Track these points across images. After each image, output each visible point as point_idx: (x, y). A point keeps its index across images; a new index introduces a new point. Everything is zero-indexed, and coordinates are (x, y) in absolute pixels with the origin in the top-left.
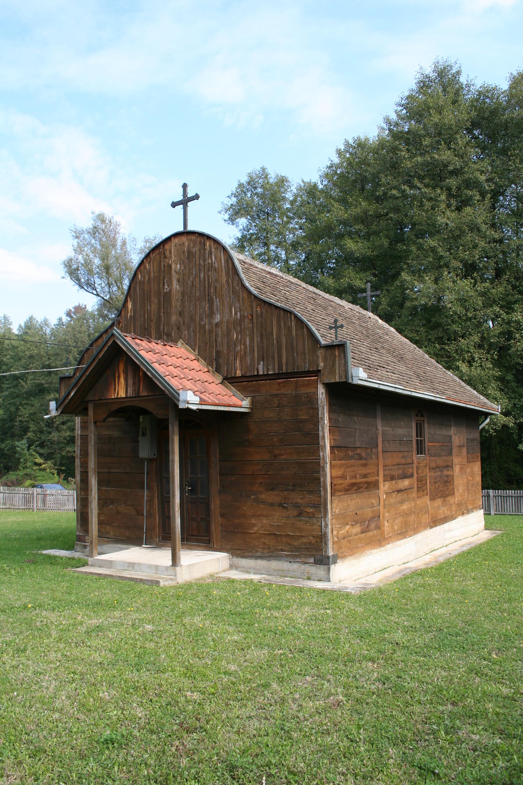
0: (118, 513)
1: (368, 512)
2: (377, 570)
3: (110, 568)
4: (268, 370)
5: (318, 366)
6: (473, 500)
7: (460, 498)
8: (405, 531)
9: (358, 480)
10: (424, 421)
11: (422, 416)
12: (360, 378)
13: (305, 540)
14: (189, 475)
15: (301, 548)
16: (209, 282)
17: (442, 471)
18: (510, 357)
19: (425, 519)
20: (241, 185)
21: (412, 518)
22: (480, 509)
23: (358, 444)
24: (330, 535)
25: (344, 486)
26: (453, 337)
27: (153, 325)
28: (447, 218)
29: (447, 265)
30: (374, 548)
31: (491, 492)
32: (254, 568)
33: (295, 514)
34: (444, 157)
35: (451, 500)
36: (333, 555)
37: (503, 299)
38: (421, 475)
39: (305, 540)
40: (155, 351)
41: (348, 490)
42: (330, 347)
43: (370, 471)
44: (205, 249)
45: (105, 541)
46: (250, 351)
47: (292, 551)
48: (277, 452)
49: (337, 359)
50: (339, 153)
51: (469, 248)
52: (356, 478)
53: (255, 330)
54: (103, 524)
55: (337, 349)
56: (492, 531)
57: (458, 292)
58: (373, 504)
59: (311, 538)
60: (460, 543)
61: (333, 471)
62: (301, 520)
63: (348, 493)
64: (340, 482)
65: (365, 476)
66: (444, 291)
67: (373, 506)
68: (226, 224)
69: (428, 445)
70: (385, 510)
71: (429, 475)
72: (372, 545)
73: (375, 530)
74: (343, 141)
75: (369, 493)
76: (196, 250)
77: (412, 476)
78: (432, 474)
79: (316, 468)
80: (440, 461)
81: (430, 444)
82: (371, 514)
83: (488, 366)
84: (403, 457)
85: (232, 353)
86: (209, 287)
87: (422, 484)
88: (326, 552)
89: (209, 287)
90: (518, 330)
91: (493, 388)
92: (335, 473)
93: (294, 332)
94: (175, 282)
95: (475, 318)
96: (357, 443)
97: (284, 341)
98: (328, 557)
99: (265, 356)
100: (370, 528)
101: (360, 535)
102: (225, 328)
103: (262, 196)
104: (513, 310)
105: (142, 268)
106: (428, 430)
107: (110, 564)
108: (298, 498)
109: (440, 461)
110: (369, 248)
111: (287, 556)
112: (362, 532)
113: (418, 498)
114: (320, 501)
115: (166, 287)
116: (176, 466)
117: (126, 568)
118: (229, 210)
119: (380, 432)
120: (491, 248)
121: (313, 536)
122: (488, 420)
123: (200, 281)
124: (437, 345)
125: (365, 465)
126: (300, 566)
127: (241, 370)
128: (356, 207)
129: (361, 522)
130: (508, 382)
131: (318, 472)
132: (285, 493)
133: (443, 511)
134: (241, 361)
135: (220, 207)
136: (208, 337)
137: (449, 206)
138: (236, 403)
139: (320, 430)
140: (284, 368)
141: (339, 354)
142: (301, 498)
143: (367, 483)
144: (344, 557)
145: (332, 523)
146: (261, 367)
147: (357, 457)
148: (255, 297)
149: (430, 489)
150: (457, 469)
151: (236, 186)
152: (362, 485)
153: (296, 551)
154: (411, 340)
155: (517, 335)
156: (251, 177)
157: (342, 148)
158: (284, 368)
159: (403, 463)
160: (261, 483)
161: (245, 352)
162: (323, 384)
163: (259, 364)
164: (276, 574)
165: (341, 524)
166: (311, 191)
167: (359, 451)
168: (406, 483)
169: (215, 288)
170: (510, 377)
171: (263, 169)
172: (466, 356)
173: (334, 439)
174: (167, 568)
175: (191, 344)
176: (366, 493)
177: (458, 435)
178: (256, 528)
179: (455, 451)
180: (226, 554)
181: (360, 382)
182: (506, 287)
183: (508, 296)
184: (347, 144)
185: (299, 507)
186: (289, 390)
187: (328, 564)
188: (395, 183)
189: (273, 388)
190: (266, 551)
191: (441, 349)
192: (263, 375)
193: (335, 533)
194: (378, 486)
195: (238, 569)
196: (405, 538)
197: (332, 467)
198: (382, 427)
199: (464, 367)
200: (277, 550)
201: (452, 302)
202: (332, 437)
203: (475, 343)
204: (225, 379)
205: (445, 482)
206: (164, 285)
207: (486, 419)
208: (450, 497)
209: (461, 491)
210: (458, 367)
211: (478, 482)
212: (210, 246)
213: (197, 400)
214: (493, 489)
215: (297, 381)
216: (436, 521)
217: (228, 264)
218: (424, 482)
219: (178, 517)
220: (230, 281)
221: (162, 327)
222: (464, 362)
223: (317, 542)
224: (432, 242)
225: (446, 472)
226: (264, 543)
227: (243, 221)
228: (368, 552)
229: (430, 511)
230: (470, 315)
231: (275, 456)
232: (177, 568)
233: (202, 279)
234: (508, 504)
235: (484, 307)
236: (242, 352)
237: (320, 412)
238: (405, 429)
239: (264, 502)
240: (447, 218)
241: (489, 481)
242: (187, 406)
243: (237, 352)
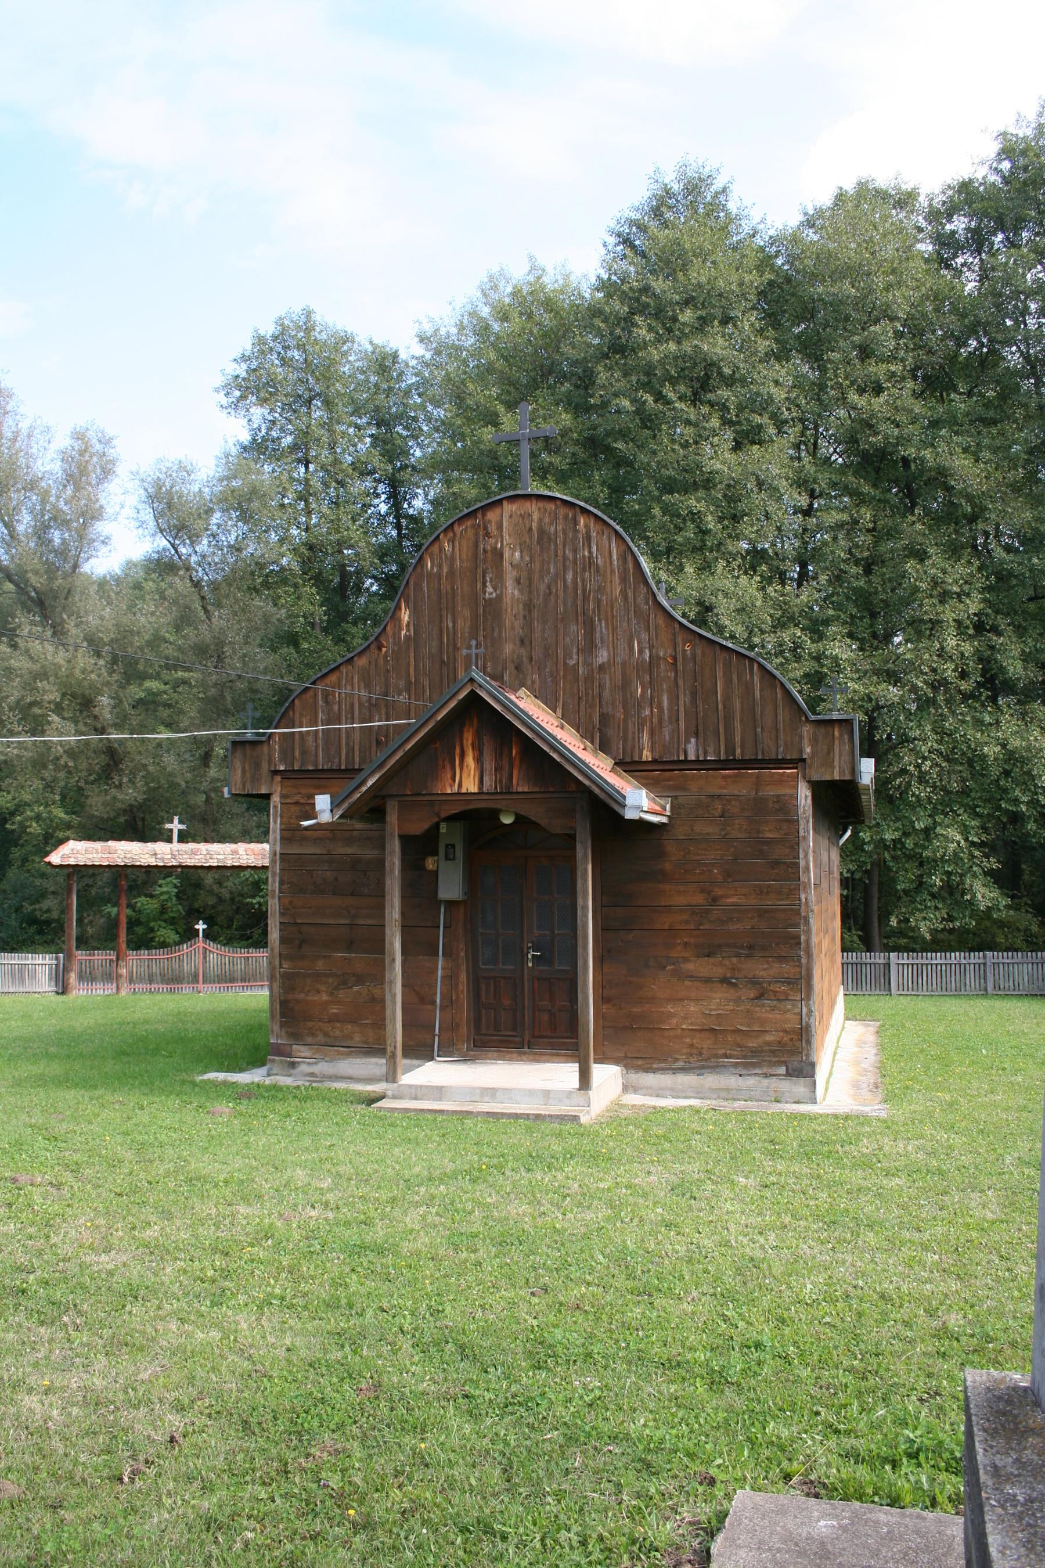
3: (440, 1099)
4: (705, 753)
5: (801, 751)
13: (769, 1038)
16: (584, 590)
44: (576, 531)
49: (837, 743)
53: (680, 683)
62: (763, 1006)
88: (807, 1055)
93: (757, 693)
108: (762, 969)
115: (489, 589)
127: (652, 751)
132: (734, 960)
139: (801, 856)
158: (738, 751)
162: (809, 782)
163: (687, 741)
174: (569, 1094)
185: (760, 983)
192: (697, 761)
200: (716, 1056)
206: (484, 585)
212: (586, 526)
215: (758, 776)
224: (694, 502)
226: (692, 1046)
237: (801, 828)
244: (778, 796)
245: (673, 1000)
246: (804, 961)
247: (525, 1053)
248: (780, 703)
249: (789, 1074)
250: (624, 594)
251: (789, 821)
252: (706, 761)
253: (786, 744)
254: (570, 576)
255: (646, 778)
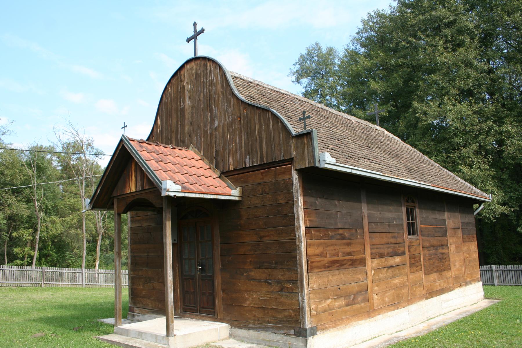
0: (154, 289)
1: (354, 287)
2: (365, 340)
4: (253, 162)
5: (291, 154)
6: (471, 274)
7: (457, 272)
8: (397, 302)
9: (341, 258)
10: (415, 207)
11: (413, 202)
12: (327, 162)
13: (286, 313)
14: (200, 257)
15: (283, 321)
16: (210, 95)
17: (436, 249)
18: (504, 159)
19: (420, 291)
20: (302, 56)
21: (405, 291)
22: (479, 281)
23: (339, 225)
24: (306, 309)
25: (323, 263)
26: (456, 148)
27: (173, 135)
28: (444, 57)
29: (447, 93)
30: (362, 319)
31: (494, 267)
32: (247, 338)
33: (278, 290)
34: (440, 13)
35: (448, 274)
36: (311, 328)
37: (494, 116)
38: (414, 253)
39: (286, 313)
40: (158, 152)
41: (328, 267)
42: (299, 136)
43: (355, 250)
44: (207, 69)
45: (146, 312)
46: (239, 147)
47: (276, 323)
48: (262, 234)
49: (306, 146)
50: (364, 21)
51: (464, 79)
52: (338, 256)
53: (242, 129)
54: (145, 298)
55: (305, 137)
56: (491, 300)
57: (457, 113)
58: (360, 279)
59: (291, 311)
60: (458, 311)
61: (309, 249)
62: (282, 295)
63: (329, 269)
64: (318, 259)
65: (349, 254)
66: (446, 113)
67: (359, 281)
68: (294, 84)
69: (421, 228)
70: (374, 284)
71: (422, 253)
72: (359, 317)
73: (362, 302)
74: (366, 14)
75: (355, 269)
76: (201, 71)
77: (403, 253)
78: (426, 252)
79: (292, 247)
80: (434, 241)
81: (422, 226)
82: (357, 288)
83: (485, 167)
84: (393, 237)
85: (227, 151)
86: (210, 99)
87: (415, 261)
88: (303, 324)
89: (210, 99)
90: (508, 138)
91: (490, 185)
92: (311, 251)
93: (271, 127)
94: (187, 99)
95: (473, 132)
96: (339, 224)
97: (264, 136)
98: (306, 330)
99: (250, 150)
100: (356, 301)
101: (344, 308)
102: (221, 130)
103: (318, 63)
104: (504, 123)
105: (166, 92)
106: (419, 214)
107: (126, 333)
108: (279, 275)
109: (434, 241)
110: (388, 86)
111: (273, 327)
112: (347, 305)
113: (411, 273)
114: (297, 277)
115: (182, 104)
116: (168, 248)
117: (137, 337)
118: (294, 74)
119: (366, 215)
120: (482, 77)
121: (293, 310)
122: (482, 207)
123: (204, 95)
124: (444, 155)
125: (349, 244)
126: (283, 338)
127: (233, 165)
128: (377, 58)
129: (346, 296)
130: (504, 180)
131: (295, 250)
132: (270, 270)
133: (440, 284)
134: (233, 157)
135: (288, 72)
136: (209, 140)
137: (446, 48)
138: (227, 192)
139: (295, 212)
140: (265, 159)
141: (308, 142)
142: (282, 275)
143: (351, 260)
144: (325, 329)
145: (309, 298)
146: (247, 161)
147: (338, 236)
148: (242, 102)
149: (424, 265)
150: (452, 248)
151: (299, 56)
152: (345, 262)
153: (280, 324)
154: (421, 151)
155: (508, 142)
156: (309, 50)
157: (366, 18)
158: (265, 159)
159: (393, 242)
160: (251, 261)
161: (236, 149)
162: (296, 170)
163: (246, 158)
164: (264, 344)
165: (320, 298)
166: (352, 55)
167: (341, 231)
168: (398, 260)
169: (214, 98)
170: (505, 176)
171: (317, 44)
172: (467, 161)
173: (309, 220)
174: (163, 337)
175: (198, 148)
176: (350, 269)
177: (452, 220)
178: (248, 302)
179: (449, 232)
180: (226, 325)
181: (327, 166)
182: (496, 106)
183: (499, 113)
184: (370, 15)
185: (281, 283)
186: (269, 179)
187: (306, 337)
188: (404, 37)
189: (257, 177)
190: (256, 322)
191: (447, 158)
192: (250, 167)
193: (313, 306)
194: (365, 263)
195: (236, 338)
196: (398, 308)
197: (308, 246)
198: (365, 210)
199: (465, 170)
200: (265, 322)
201: (453, 120)
202: (307, 219)
203: (474, 151)
204: (222, 173)
205: (440, 258)
206: (180, 103)
207: (480, 206)
208: (446, 272)
209: (457, 266)
210: (461, 169)
211: (475, 259)
212: (210, 66)
213: (179, 188)
214: (495, 264)
215: (275, 171)
216: (432, 293)
217: (222, 78)
218: (418, 259)
219: (171, 292)
220: (224, 92)
221: (179, 136)
222: (466, 166)
223: (296, 315)
224: (434, 77)
225: (440, 250)
226: (255, 316)
227: (305, 81)
228: (354, 323)
229: (424, 284)
230: (468, 129)
231: (261, 238)
232: (170, 338)
233: (205, 94)
234: (509, 276)
235: (480, 123)
236: (234, 150)
237: (294, 196)
238: (398, 213)
239: (254, 279)
240: (444, 57)
241: (485, 259)
242: (167, 193)
243: (230, 150)
244: (284, 180)
245: (248, 291)
246: (299, 270)
247: (197, 315)
248: (281, 130)
249: (295, 335)
250: (222, 92)
251: (289, 193)
252: (253, 166)
253: (284, 152)
254: (205, 90)
255: (231, 178)
